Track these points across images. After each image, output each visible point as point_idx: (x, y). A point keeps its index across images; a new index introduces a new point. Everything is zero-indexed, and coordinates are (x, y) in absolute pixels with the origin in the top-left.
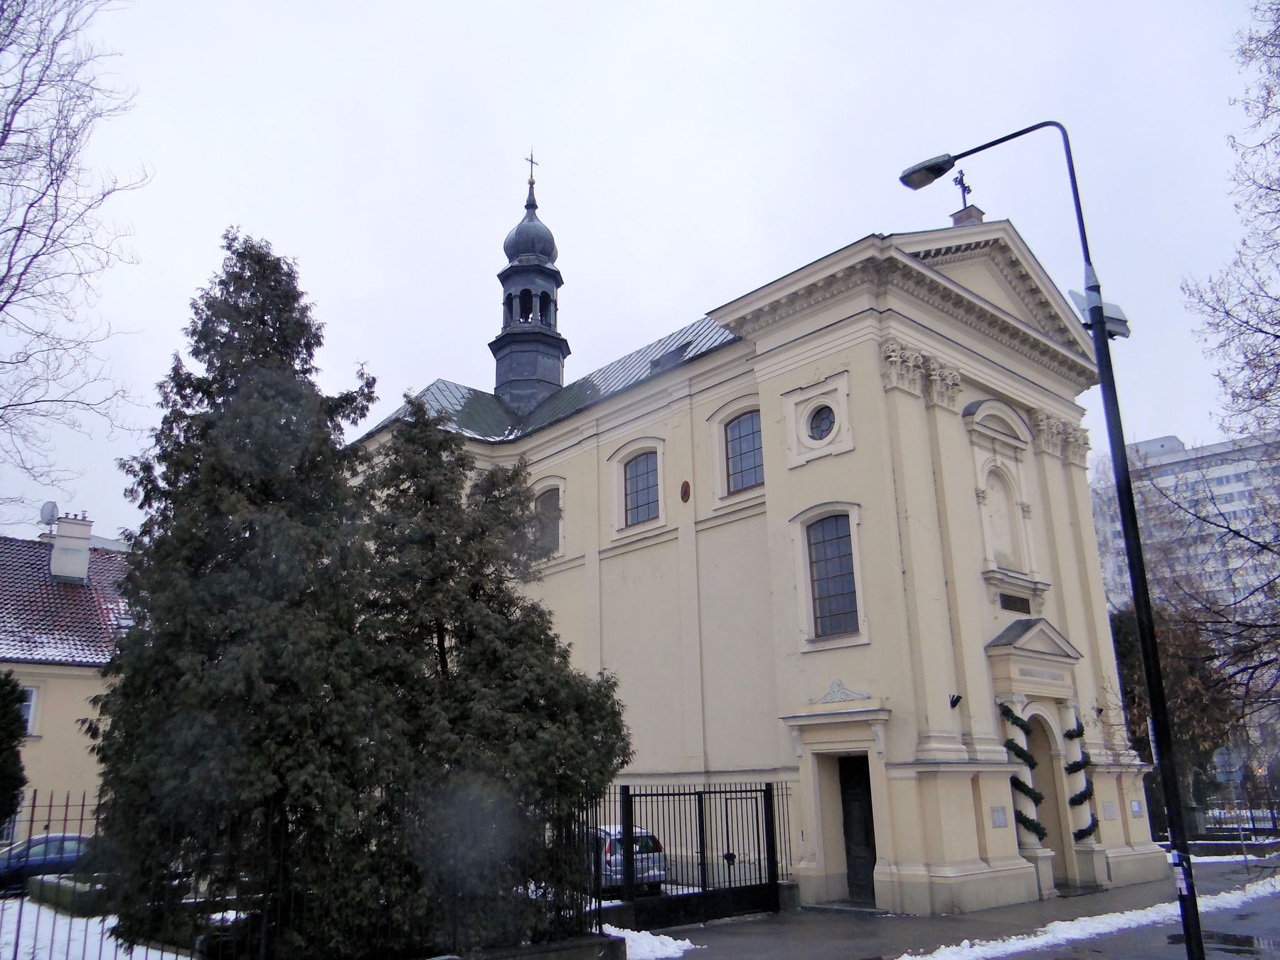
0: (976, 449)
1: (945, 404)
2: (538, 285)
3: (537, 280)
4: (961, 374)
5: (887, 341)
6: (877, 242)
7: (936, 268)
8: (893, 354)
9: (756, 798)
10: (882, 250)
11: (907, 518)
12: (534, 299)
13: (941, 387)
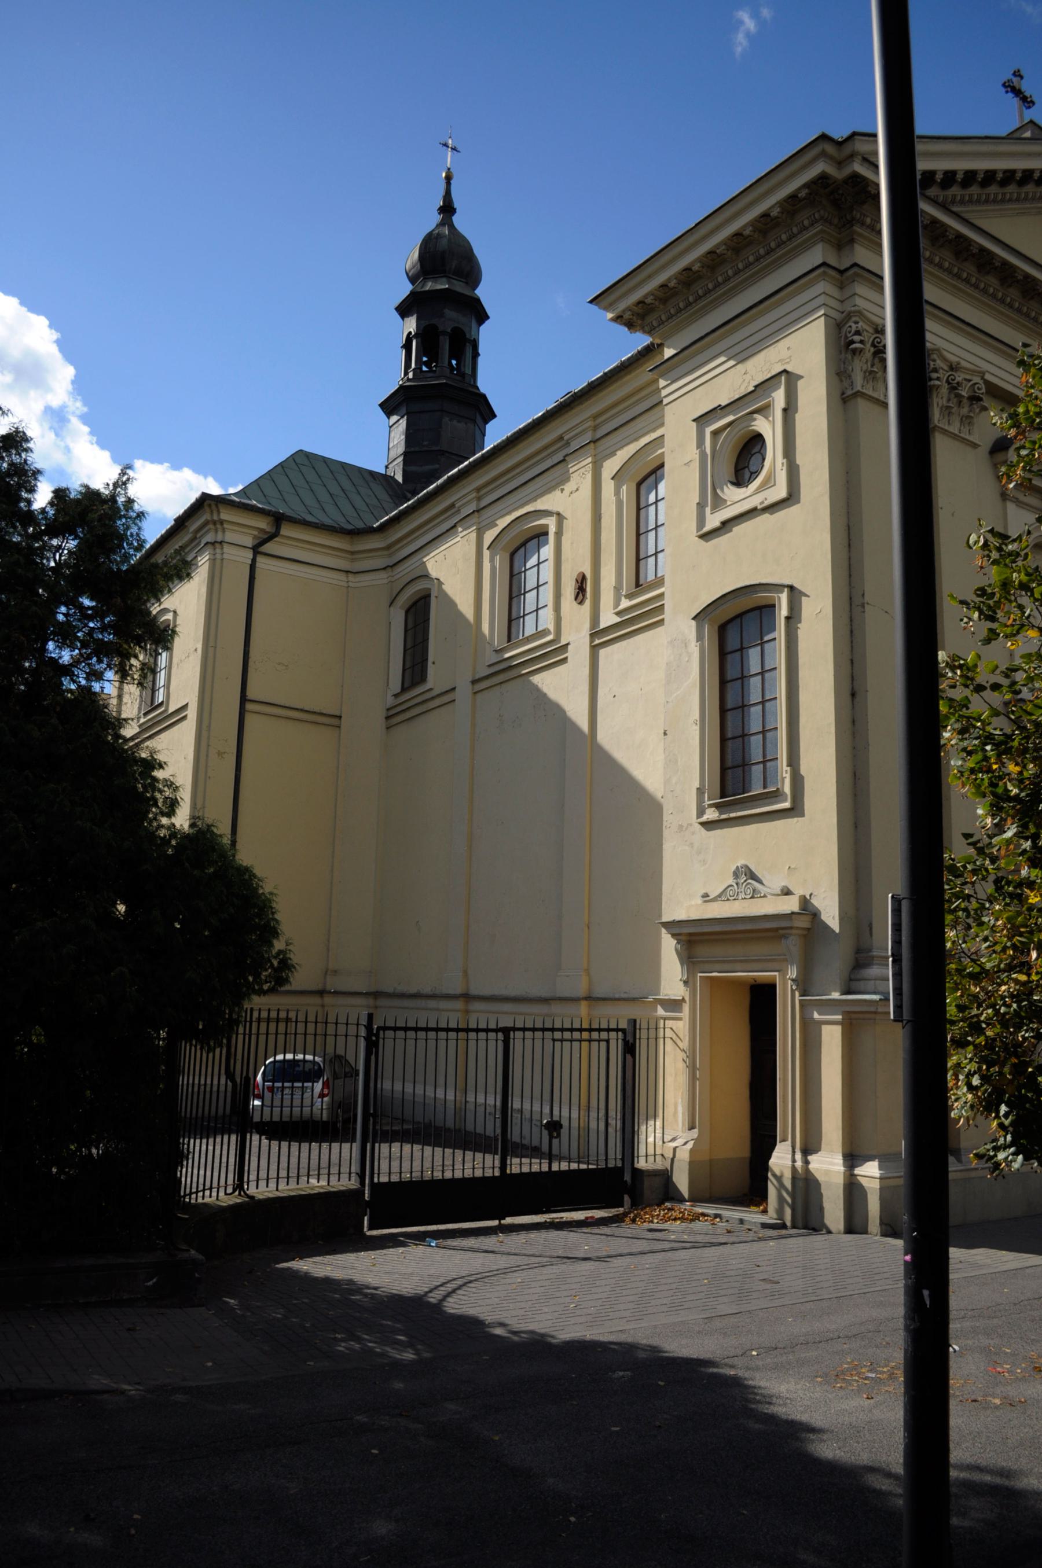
0: (1011, 507)
1: (954, 428)
2: (451, 318)
3: (447, 311)
4: (987, 383)
5: (849, 316)
6: (830, 149)
7: (955, 209)
8: (857, 338)
9: (608, 1041)
10: (840, 164)
11: (863, 606)
12: (441, 338)
13: (949, 400)
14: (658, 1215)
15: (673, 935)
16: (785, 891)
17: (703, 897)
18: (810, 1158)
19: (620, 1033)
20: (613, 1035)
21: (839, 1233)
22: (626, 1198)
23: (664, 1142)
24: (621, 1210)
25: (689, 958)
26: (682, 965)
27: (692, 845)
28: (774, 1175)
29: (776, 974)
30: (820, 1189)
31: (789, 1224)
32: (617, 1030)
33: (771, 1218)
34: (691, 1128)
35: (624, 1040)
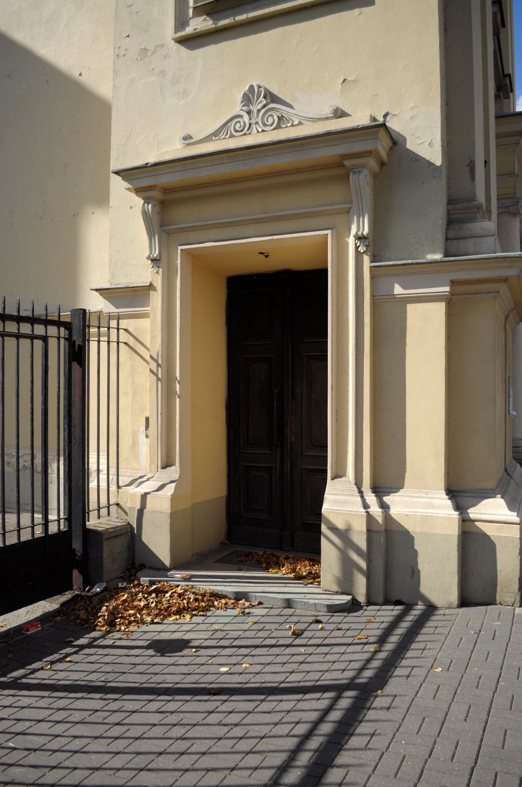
9: (45, 339)
14: (147, 606)
15: (138, 191)
16: (339, 113)
17: (185, 138)
18: (386, 499)
19: (62, 329)
20: (52, 330)
21: (449, 608)
22: (76, 574)
23: (119, 487)
24: (67, 596)
25: (161, 226)
26: (151, 235)
27: (163, 73)
28: (334, 529)
29: (329, 232)
30: (413, 544)
31: (362, 599)
32: (58, 324)
33: (327, 592)
34: (166, 466)
35: (69, 339)
